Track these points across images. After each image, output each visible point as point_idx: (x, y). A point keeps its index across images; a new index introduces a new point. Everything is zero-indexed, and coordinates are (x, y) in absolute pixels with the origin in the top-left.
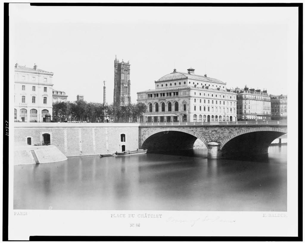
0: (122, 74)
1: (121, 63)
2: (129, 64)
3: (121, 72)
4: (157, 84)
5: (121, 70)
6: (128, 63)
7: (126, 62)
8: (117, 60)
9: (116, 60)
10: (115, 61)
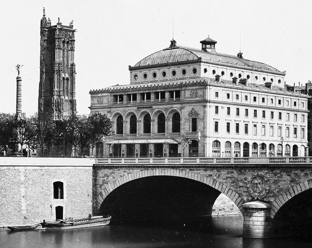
0: (57, 51)
1: (56, 26)
2: (74, 29)
3: (55, 45)
4: (134, 73)
5: (54, 42)
6: (71, 27)
7: (66, 23)
8: (47, 19)
10: (42, 22)
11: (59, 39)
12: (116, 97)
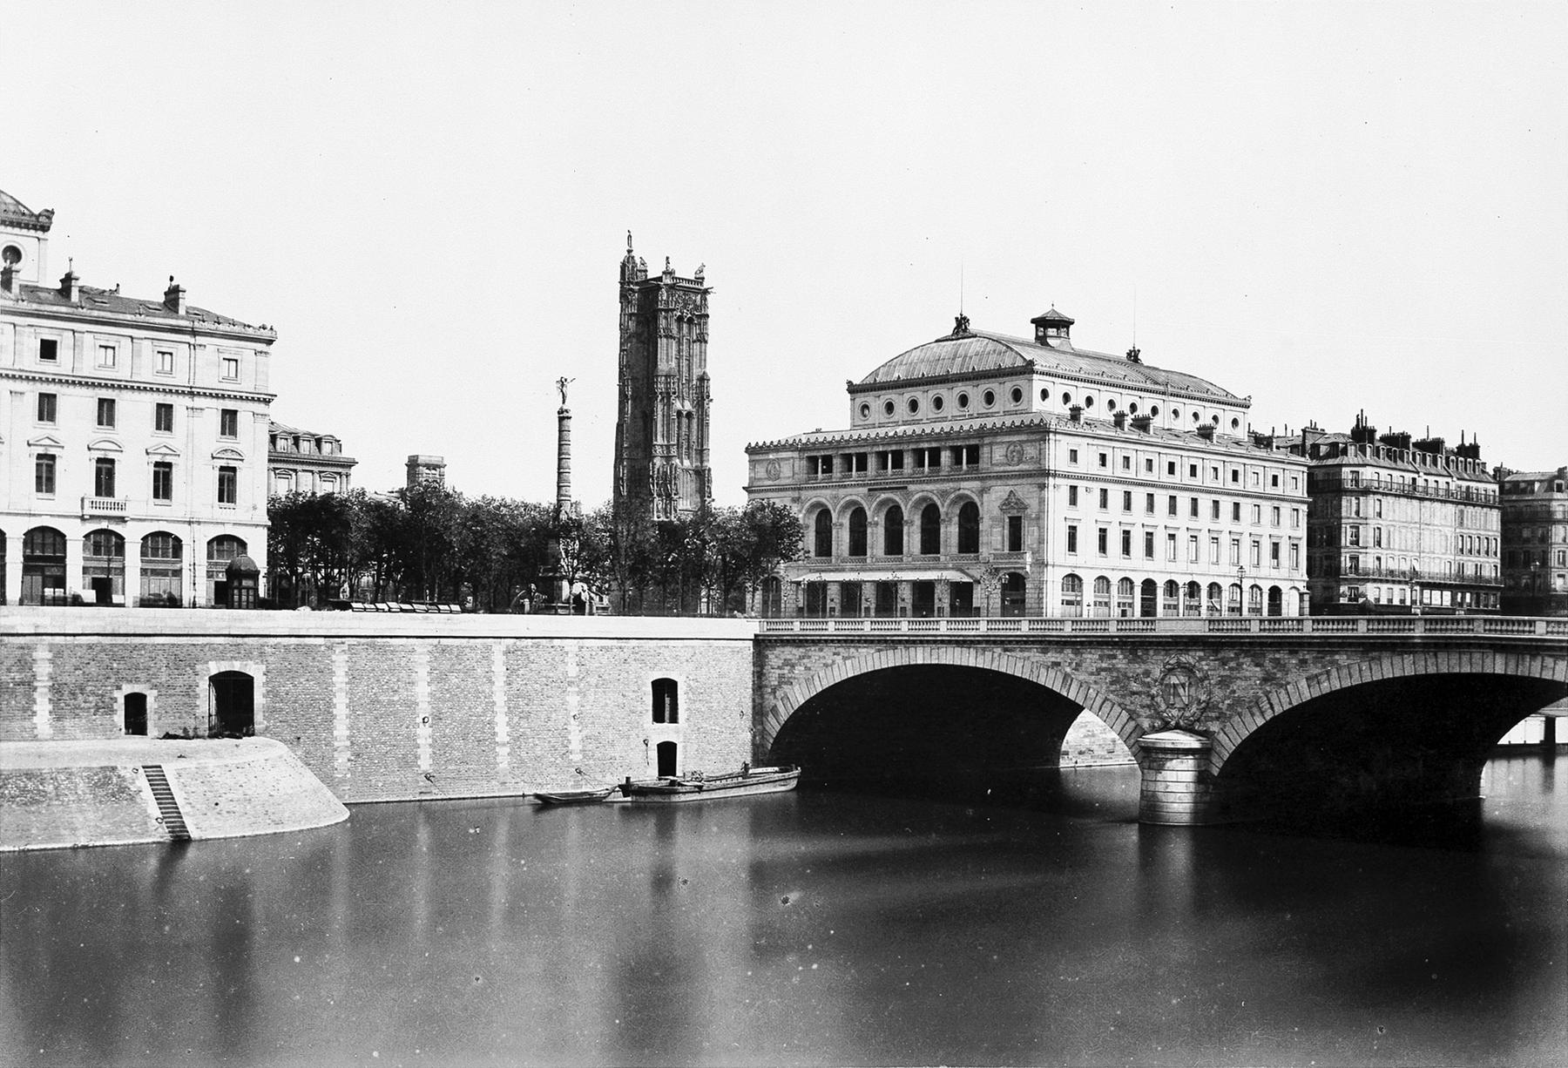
0: (662, 342)
1: (660, 279)
2: (706, 286)
4: (861, 399)
5: (656, 319)
7: (685, 271)
8: (638, 261)
9: (630, 258)
10: (623, 267)
11: (667, 311)
12: (813, 461)
